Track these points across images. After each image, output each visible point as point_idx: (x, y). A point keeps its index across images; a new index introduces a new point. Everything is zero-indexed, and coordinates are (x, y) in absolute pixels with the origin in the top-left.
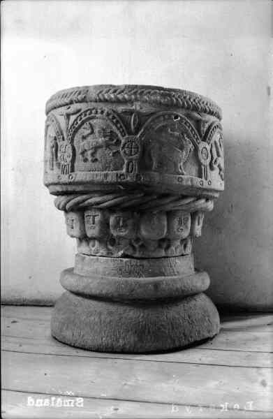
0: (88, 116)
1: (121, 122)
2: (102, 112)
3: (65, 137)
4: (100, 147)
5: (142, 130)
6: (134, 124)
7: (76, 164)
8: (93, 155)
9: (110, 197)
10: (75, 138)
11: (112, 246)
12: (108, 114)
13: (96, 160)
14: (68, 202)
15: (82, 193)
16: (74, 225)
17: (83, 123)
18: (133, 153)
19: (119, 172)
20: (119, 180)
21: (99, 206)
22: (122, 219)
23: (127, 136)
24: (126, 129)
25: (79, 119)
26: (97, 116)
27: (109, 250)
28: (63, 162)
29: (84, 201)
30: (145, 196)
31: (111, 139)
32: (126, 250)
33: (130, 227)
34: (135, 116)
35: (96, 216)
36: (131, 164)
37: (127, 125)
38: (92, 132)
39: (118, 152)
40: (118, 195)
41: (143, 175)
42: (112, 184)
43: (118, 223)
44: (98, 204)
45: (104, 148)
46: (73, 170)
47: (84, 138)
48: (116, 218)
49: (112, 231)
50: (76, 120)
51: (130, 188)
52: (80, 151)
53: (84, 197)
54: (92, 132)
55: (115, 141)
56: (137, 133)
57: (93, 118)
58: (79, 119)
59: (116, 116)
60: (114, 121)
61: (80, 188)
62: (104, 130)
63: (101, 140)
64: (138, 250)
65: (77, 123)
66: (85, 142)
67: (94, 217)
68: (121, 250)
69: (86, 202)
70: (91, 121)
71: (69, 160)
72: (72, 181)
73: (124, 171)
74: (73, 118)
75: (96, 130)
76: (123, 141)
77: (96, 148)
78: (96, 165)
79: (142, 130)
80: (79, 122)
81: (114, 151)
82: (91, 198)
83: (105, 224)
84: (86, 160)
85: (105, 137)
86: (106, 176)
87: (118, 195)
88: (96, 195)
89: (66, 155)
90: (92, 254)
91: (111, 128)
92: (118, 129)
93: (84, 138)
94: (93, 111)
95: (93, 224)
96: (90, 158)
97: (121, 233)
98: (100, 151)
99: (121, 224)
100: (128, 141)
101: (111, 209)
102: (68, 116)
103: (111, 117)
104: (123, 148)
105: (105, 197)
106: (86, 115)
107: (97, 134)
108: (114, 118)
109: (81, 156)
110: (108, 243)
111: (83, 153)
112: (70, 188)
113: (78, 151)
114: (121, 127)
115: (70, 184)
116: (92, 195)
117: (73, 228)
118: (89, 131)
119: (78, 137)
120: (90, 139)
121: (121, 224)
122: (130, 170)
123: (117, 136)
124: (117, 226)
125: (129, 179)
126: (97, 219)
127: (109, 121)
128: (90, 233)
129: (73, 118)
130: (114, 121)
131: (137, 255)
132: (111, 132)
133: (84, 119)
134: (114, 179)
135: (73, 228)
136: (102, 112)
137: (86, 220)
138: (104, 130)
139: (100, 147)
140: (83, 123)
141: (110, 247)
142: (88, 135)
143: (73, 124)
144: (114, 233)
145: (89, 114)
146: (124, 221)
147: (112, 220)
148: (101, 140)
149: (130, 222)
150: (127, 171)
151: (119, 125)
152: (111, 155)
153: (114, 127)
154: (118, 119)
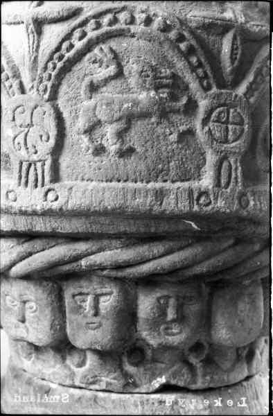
0: (105, 29)
1: (200, 51)
2: (148, 21)
3: (27, 85)
4: (145, 115)
5: (251, 78)
6: (233, 59)
7: (65, 161)
8: (120, 135)
9: (158, 248)
10: (64, 88)
11: (136, 365)
12: (166, 29)
13: (131, 151)
14: (22, 259)
15: (73, 238)
16: (29, 315)
17: (88, 48)
18: (230, 137)
19: (195, 184)
20: (196, 208)
21: (120, 274)
22: (172, 302)
23: (214, 90)
24: (213, 74)
25: (77, 34)
26: (133, 29)
27: (126, 375)
28: (23, 152)
29: (77, 258)
30: (235, 244)
31: (174, 97)
32: (174, 375)
33: (193, 322)
34: (235, 38)
35: (103, 295)
36: (225, 164)
37: (213, 58)
38: (119, 74)
39: (190, 132)
40: (184, 243)
41: (254, 194)
42: (176, 218)
43: (163, 312)
44: (119, 267)
45: (153, 120)
46: (56, 177)
47: (93, 88)
48: (158, 299)
49: (145, 333)
50: (68, 36)
51: (212, 228)
52: (81, 123)
53: (82, 247)
54: (119, 74)
55: (184, 100)
56: (236, 84)
57: (121, 34)
58: (77, 34)
59: (186, 34)
60: (183, 46)
61: (66, 227)
62: (154, 69)
63: (145, 97)
64: (199, 372)
65: (72, 46)
66: (97, 97)
67: (97, 298)
68: (160, 375)
69: (83, 262)
70: (113, 44)
71: (45, 147)
72: (55, 205)
73: (207, 181)
74: (53, 34)
75: (132, 67)
76: (203, 104)
77: (129, 120)
78: (132, 163)
79: (251, 78)
80: (79, 45)
81: (182, 128)
82: (100, 250)
83: (127, 315)
84: (100, 151)
85: (157, 88)
86: (160, 195)
87: (184, 243)
88: (114, 243)
89: (34, 133)
90: (77, 383)
91: (171, 65)
92: (193, 69)
93: (93, 88)
94: (123, 17)
95: (96, 314)
96: (112, 147)
97: (170, 338)
98: (139, 127)
99: (171, 314)
100: (219, 103)
101: (150, 281)
102: (39, 25)
103: (172, 35)
104: (205, 121)
105: (143, 250)
106: (98, 26)
107: (133, 81)
108: (181, 38)
109: (85, 139)
110: (125, 359)
111: (90, 131)
112: (40, 225)
113: (76, 126)
114: (200, 65)
115: (47, 213)
116: (106, 242)
117: (23, 321)
118: (112, 69)
119: (73, 86)
120: (107, 92)
121: (171, 314)
122: (223, 181)
123: (187, 88)
124: (159, 319)
125: (221, 203)
126: (107, 303)
127: (166, 46)
128: (81, 339)
129: (53, 34)
130: (183, 46)
131: (200, 384)
132: (174, 76)
133: (92, 35)
134: (184, 206)
135: (23, 321)
136: (148, 21)
137: (68, 300)
138: (154, 69)
139: (145, 115)
140: (88, 48)
141: (130, 369)
142: (106, 81)
143: (58, 49)
144: (152, 339)
145: (110, 24)
146: (180, 308)
147: (146, 304)
148: (145, 97)
149: (193, 308)
150: (218, 184)
151: (194, 60)
152: (174, 137)
153: (180, 65)
154: (193, 42)
